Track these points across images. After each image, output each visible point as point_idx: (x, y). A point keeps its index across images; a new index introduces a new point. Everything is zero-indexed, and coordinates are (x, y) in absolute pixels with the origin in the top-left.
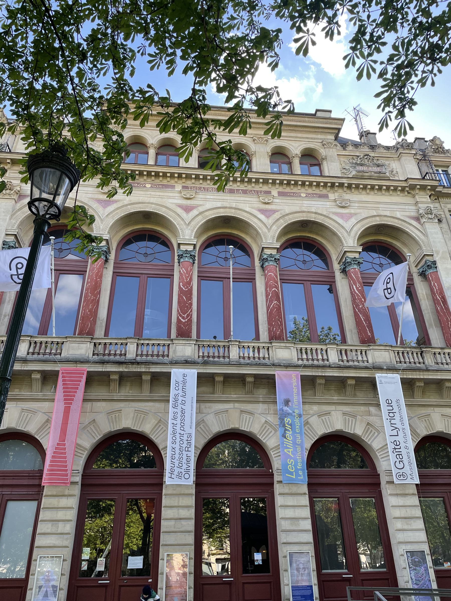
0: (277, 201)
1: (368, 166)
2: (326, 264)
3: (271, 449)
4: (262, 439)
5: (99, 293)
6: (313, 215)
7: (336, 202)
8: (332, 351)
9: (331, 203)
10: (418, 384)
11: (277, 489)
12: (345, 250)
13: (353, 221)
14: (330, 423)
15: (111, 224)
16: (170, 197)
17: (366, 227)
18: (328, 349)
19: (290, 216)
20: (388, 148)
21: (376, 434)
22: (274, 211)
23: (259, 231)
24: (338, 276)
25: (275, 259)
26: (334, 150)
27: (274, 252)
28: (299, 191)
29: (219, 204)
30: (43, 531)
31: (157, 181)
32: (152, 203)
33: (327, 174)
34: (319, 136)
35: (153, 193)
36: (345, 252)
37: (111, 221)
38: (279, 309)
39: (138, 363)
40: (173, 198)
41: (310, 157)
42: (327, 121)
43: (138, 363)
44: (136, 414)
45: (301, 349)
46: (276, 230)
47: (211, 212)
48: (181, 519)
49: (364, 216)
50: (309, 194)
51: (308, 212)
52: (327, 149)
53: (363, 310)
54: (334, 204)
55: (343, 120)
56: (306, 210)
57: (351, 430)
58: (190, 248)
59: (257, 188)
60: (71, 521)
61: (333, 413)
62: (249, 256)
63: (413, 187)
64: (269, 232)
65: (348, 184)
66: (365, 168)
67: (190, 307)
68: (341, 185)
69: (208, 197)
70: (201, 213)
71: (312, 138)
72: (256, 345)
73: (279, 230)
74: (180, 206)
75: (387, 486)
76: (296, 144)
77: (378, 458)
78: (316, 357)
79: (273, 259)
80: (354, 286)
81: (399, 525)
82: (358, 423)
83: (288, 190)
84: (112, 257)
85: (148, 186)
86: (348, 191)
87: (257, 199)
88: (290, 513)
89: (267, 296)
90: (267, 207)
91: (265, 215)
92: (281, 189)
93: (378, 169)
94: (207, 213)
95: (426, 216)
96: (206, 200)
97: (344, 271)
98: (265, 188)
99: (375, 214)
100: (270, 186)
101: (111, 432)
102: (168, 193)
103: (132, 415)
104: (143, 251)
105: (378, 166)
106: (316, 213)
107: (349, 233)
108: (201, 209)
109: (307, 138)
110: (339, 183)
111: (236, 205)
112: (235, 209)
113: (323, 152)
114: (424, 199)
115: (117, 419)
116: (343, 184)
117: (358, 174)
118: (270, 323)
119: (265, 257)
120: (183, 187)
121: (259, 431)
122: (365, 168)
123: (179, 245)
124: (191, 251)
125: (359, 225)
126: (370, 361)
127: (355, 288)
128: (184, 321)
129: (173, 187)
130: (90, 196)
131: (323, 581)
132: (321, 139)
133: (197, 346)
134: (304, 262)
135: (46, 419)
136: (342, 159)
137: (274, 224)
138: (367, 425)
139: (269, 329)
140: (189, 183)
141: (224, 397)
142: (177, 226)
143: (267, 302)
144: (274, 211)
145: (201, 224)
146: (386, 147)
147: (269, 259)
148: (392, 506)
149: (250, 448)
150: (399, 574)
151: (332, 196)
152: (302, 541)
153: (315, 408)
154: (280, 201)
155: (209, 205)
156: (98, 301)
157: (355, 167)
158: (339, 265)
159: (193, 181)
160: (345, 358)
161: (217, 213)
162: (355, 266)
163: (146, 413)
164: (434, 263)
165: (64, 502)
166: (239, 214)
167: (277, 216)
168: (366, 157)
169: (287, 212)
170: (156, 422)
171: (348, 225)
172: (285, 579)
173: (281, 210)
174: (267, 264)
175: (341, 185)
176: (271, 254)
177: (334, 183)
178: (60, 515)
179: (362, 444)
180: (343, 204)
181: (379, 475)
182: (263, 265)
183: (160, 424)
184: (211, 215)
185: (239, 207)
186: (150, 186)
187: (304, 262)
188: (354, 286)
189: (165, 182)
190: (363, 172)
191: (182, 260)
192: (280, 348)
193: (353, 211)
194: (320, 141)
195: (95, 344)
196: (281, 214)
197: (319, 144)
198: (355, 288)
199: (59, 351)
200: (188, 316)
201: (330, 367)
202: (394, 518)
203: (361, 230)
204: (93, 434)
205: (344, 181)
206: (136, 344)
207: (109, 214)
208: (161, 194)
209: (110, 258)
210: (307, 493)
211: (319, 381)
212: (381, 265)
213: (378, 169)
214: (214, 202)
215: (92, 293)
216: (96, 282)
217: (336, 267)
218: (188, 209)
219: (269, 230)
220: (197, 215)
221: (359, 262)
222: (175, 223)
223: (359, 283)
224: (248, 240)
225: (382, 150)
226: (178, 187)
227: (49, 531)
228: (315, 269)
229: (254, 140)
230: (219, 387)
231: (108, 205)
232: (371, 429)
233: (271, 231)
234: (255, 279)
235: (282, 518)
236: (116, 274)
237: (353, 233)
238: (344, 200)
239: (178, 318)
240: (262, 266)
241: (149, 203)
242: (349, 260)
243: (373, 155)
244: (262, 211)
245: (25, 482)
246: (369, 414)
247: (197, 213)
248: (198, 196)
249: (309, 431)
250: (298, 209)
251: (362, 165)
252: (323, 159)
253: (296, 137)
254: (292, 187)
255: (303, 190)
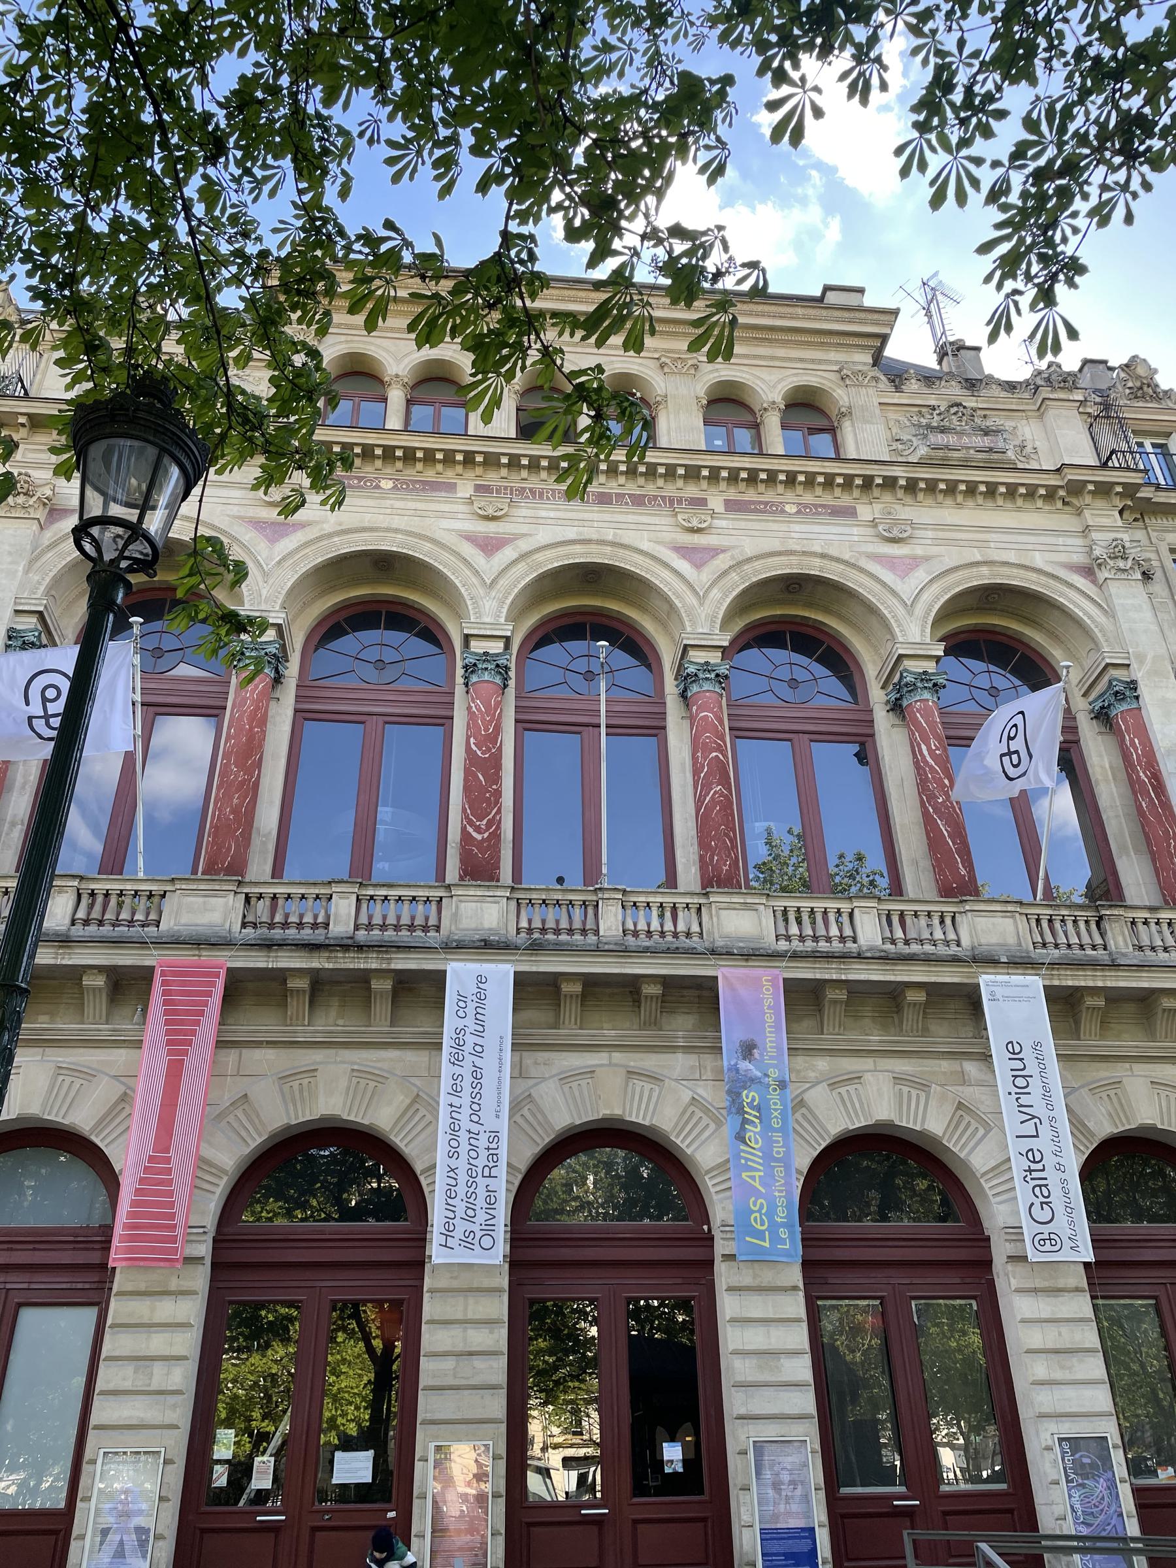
0: (723, 523)
1: (961, 434)
2: (851, 688)
3: (708, 1172)
4: (683, 1146)
5: (259, 764)
6: (817, 562)
7: (875, 526)
8: (865, 917)
9: (862, 531)
10: (1089, 1001)
11: (723, 1275)
12: (901, 652)
13: (921, 576)
14: (861, 1104)
15: (289, 584)
16: (442, 515)
17: (953, 592)
18: (856, 911)
19: (757, 564)
20: (1011, 386)
21: (981, 1131)
22: (715, 551)
23: (676, 602)
24: (882, 719)
25: (717, 675)
26: (871, 391)
27: (715, 658)
28: (780, 499)
29: (571, 533)
30: (111, 1387)
31: (410, 473)
32: (396, 531)
33: (852, 455)
34: (833, 355)
35: (398, 504)
36: (901, 657)
37: (289, 577)
38: (727, 806)
39: (360, 948)
40: (452, 516)
41: (808, 409)
42: (852, 315)
43: (360, 948)
44: (355, 1080)
45: (785, 912)
46: (721, 599)
47: (549, 554)
48: (471, 1354)
49: (950, 563)
50: (806, 506)
51: (804, 553)
52: (852, 390)
53: (947, 808)
54: (870, 531)
55: (895, 313)
56: (798, 548)
57: (915, 1123)
58: (496, 647)
59: (670, 490)
60: (185, 1358)
61: (868, 1077)
62: (649, 667)
63: (1076, 488)
64: (701, 604)
65: (908, 479)
66: (951, 439)
67: (497, 802)
68: (890, 483)
69: (543, 514)
70: (523, 556)
71: (813, 361)
72: (668, 900)
73: (729, 600)
74: (470, 538)
75: (1010, 1267)
76: (771, 376)
77: (986, 1196)
78: (823, 933)
79: (713, 676)
80: (924, 747)
81: (1040, 1369)
82: (933, 1103)
83: (751, 495)
84: (292, 669)
85: (387, 484)
86: (908, 499)
87: (671, 520)
88: (755, 1338)
89: (696, 772)
90: (697, 539)
91: (690, 561)
92: (732, 494)
93: (986, 442)
94: (539, 557)
95: (1111, 562)
96: (537, 521)
97: (896, 707)
98: (691, 490)
99: (979, 558)
100: (704, 484)
101: (289, 1127)
102: (438, 504)
103: (343, 1083)
104: (372, 654)
105: (986, 432)
106: (823, 556)
107: (910, 608)
108: (524, 545)
109: (801, 360)
110: (885, 478)
111: (615, 535)
112: (613, 544)
113: (842, 396)
114: (1105, 520)
115: (306, 1094)
116: (895, 479)
117: (933, 453)
118: (703, 844)
119: (692, 669)
120: (478, 488)
121: (677, 1124)
122: (951, 439)
123: (467, 638)
124: (497, 655)
125: (935, 588)
126: (965, 942)
127: (925, 752)
128: (479, 837)
129: (452, 487)
130: (235, 510)
131: (843, 1516)
132: (837, 363)
133: (513, 904)
134: (793, 683)
135: (120, 1093)
136: (893, 415)
137: (714, 583)
138: (958, 1108)
139: (702, 858)
140: (493, 478)
141: (585, 1035)
142: (463, 590)
143: (695, 788)
144: (715, 551)
145: (523, 583)
146: (1007, 382)
147: (701, 676)
148: (1023, 1321)
149: (653, 1168)
150: (1039, 1497)
151: (865, 512)
152: (788, 1410)
153: (822, 1064)
154: (730, 524)
155: (544, 536)
156: (257, 785)
157: (925, 436)
158: (883, 692)
159: (504, 472)
160: (899, 934)
161: (567, 556)
162: (926, 695)
163: (379, 1078)
164: (1133, 685)
165: (166, 1309)
166: (623, 560)
167: (721, 562)
168: (955, 409)
169: (749, 553)
170: (408, 1101)
171: (907, 587)
172: (742, 1509)
173: (733, 547)
174: (695, 688)
175: (890, 483)
176: (707, 663)
177: (872, 477)
178: (158, 1343)
179: (944, 1158)
180: (895, 533)
181: (988, 1239)
182: (685, 690)
183: (417, 1106)
184: (551, 560)
185: (622, 541)
186: (390, 484)
187: (793, 684)
188: (924, 747)
189: (430, 474)
190: (947, 448)
191: (474, 679)
192: (731, 907)
193: (919, 551)
194: (836, 368)
195: (248, 899)
196: (733, 557)
197: (832, 376)
198: (925, 752)
199: (153, 916)
200: (489, 825)
201: (859, 956)
202: (1029, 1351)
203: (943, 600)
204: (244, 1134)
205: (897, 471)
206: (354, 897)
207: (284, 559)
208: (420, 506)
209: (286, 673)
210: (801, 1286)
211: (831, 994)
212: (993, 692)
213: (986, 442)
214: (557, 528)
215: (241, 765)
216: (251, 736)
217: (877, 696)
218: (489, 546)
219: (701, 599)
220: (514, 562)
221: (935, 685)
222: (457, 582)
223: (937, 737)
224: (648, 625)
225: (996, 391)
226: (465, 489)
227: (127, 1385)
228: (821, 701)
229: (662, 366)
230: (571, 1010)
231: (282, 536)
232: (967, 1118)
233: (707, 602)
234: (664, 728)
235: (735, 1352)
236: (302, 715)
237: (920, 609)
238: (897, 522)
239: (464, 829)
240: (683, 695)
241: (388, 530)
242: (909, 679)
243: (974, 405)
244: (684, 551)
245: (66, 1257)
246: (963, 1079)
247: (515, 555)
248: (515, 512)
249: (805, 1124)
250: (776, 545)
251: (943, 430)
252: (843, 415)
253: (773, 358)
254: (761, 487)
255: (790, 496)
